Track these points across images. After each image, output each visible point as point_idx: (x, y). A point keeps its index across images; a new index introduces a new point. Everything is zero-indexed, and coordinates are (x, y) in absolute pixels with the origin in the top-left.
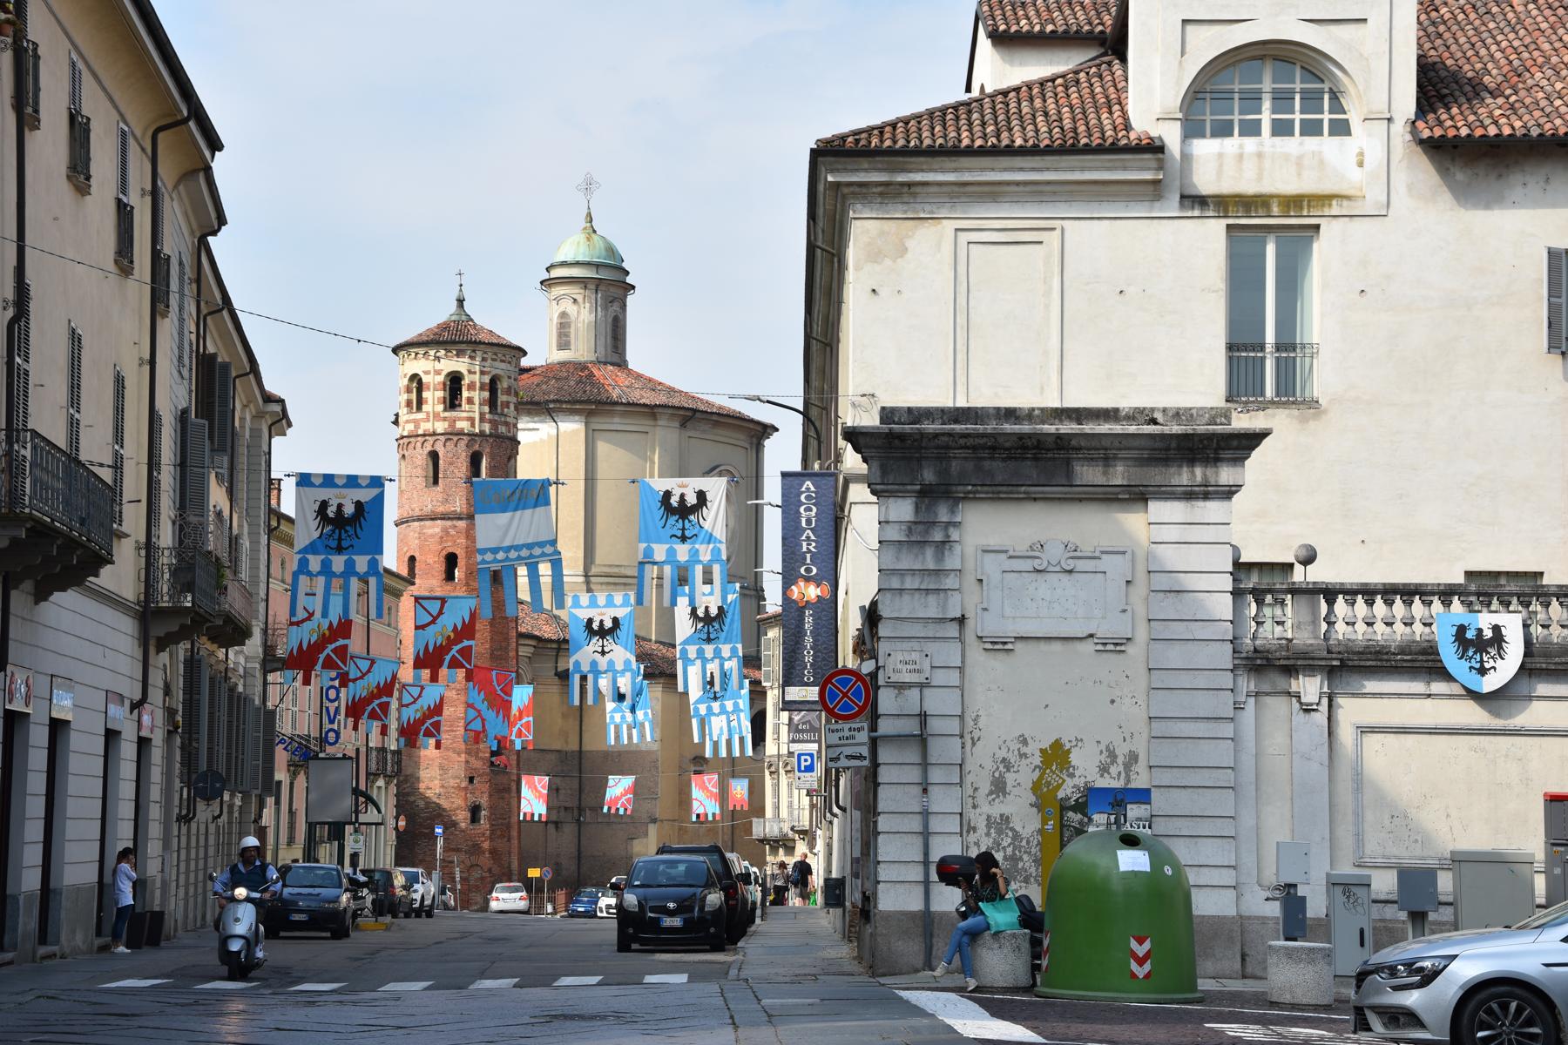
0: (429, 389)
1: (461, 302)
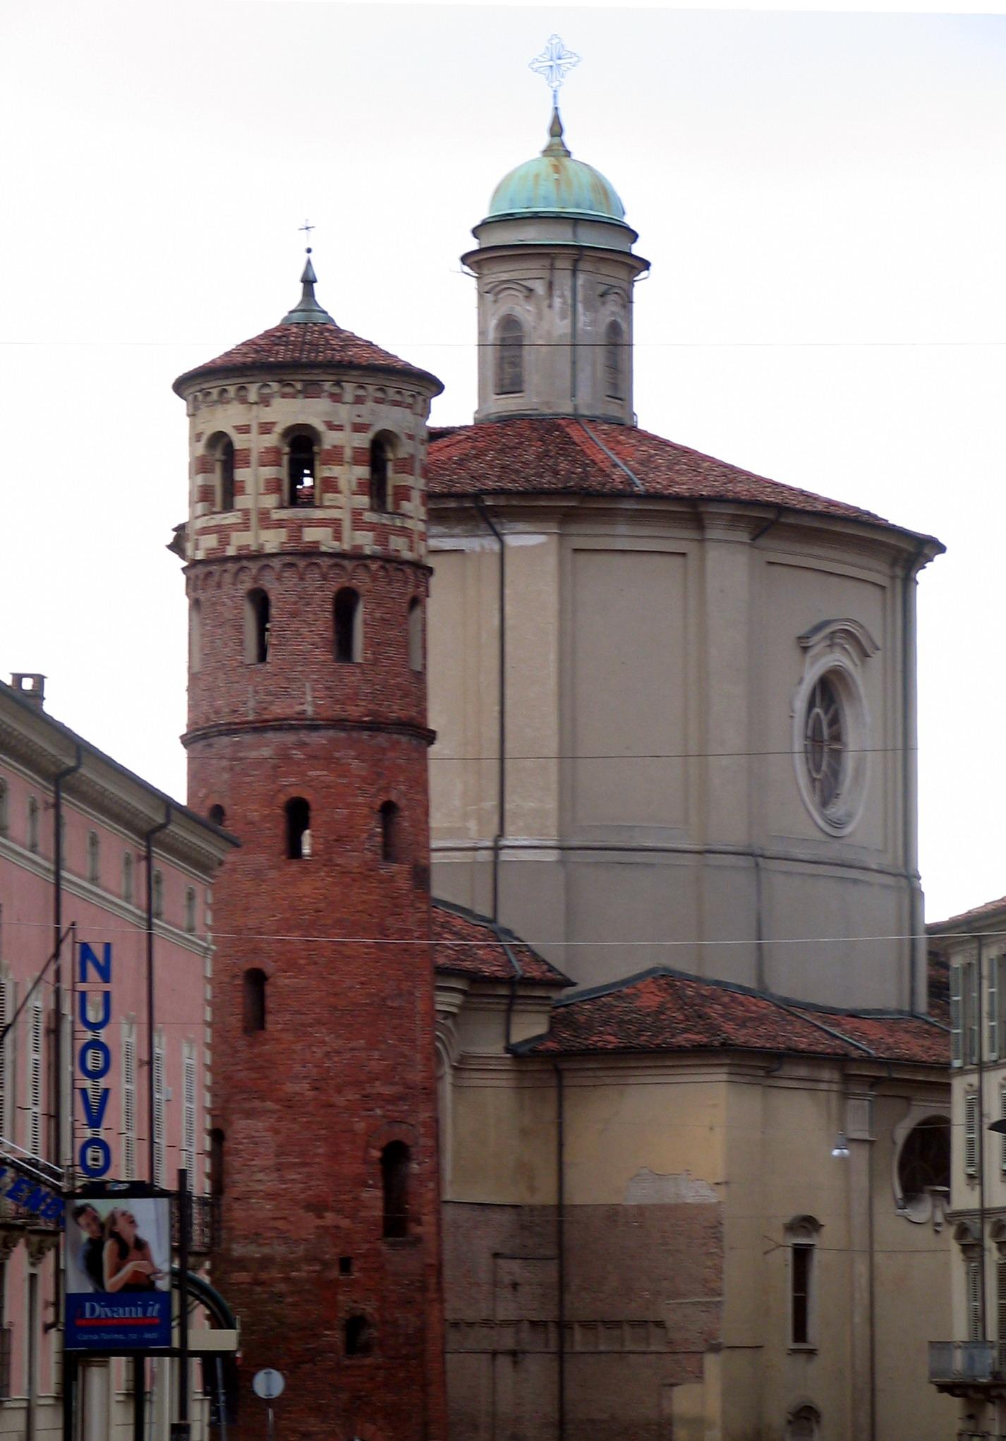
0: (247, 464)
1: (308, 282)
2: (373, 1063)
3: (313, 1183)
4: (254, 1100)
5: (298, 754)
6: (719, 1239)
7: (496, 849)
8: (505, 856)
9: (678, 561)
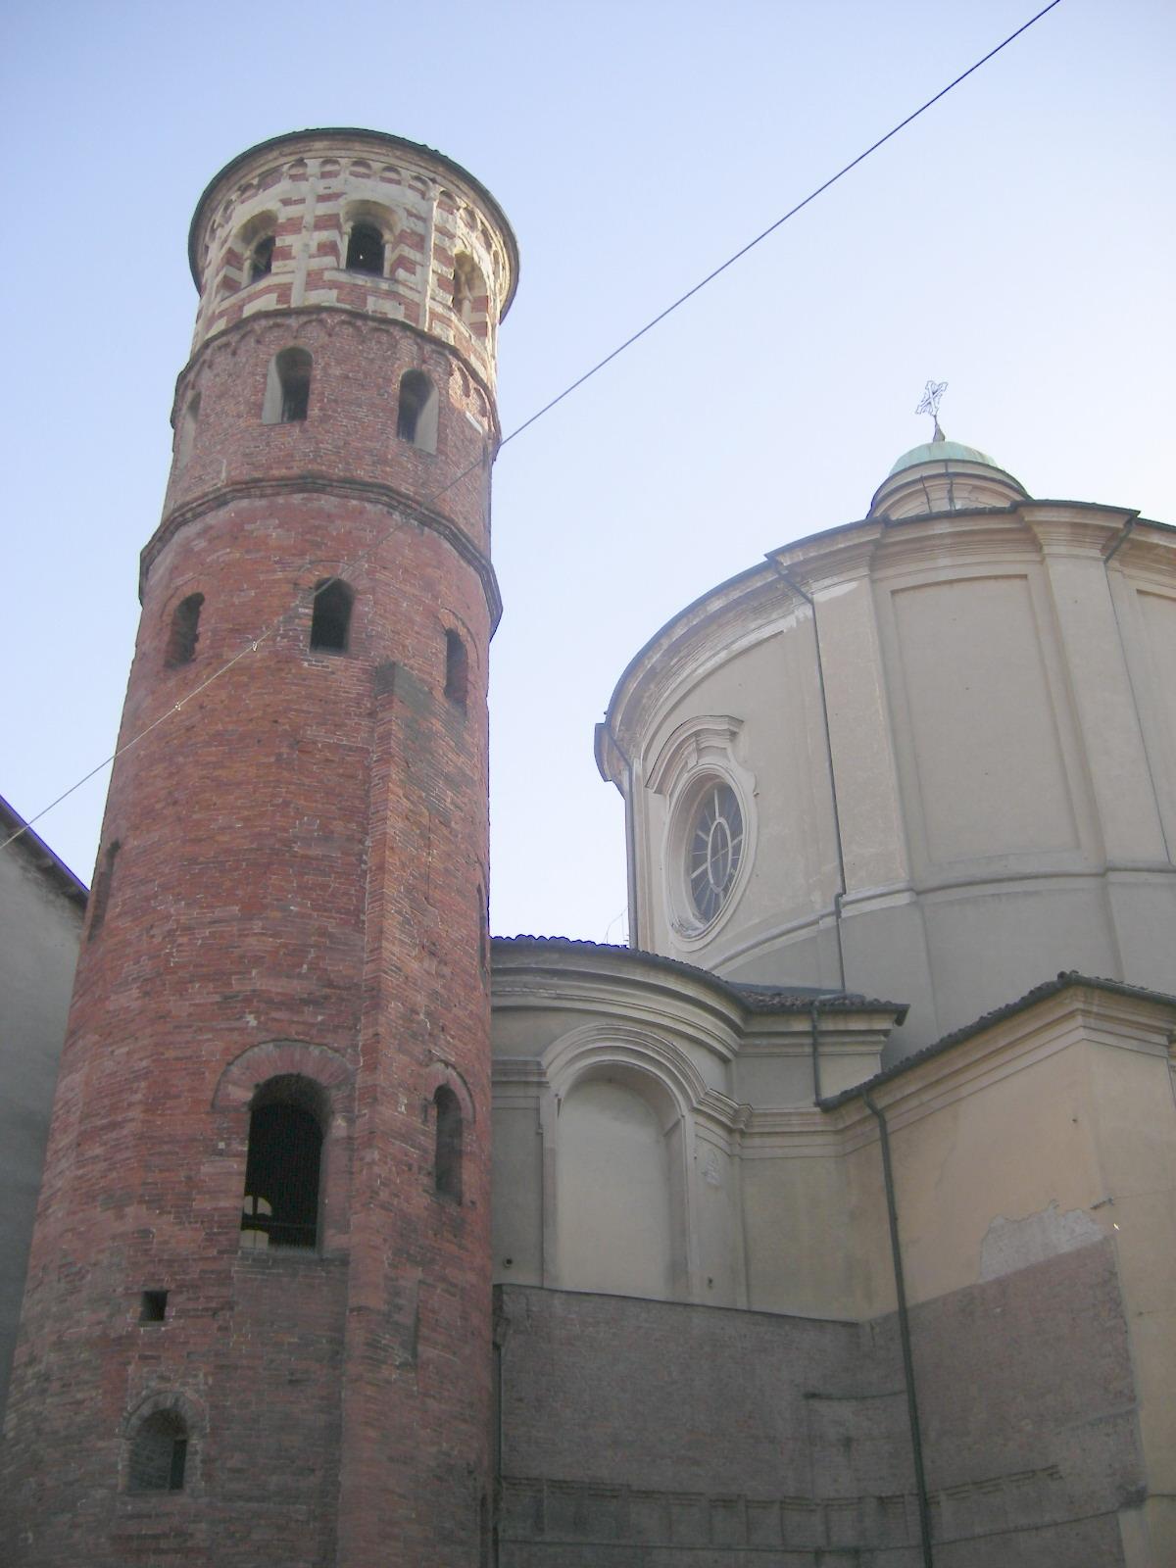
2: (252, 940)
3: (119, 1157)
4: (470, 1175)
5: (201, 544)
6: (1115, 1304)
7: (838, 913)
8: (845, 914)
9: (1018, 583)
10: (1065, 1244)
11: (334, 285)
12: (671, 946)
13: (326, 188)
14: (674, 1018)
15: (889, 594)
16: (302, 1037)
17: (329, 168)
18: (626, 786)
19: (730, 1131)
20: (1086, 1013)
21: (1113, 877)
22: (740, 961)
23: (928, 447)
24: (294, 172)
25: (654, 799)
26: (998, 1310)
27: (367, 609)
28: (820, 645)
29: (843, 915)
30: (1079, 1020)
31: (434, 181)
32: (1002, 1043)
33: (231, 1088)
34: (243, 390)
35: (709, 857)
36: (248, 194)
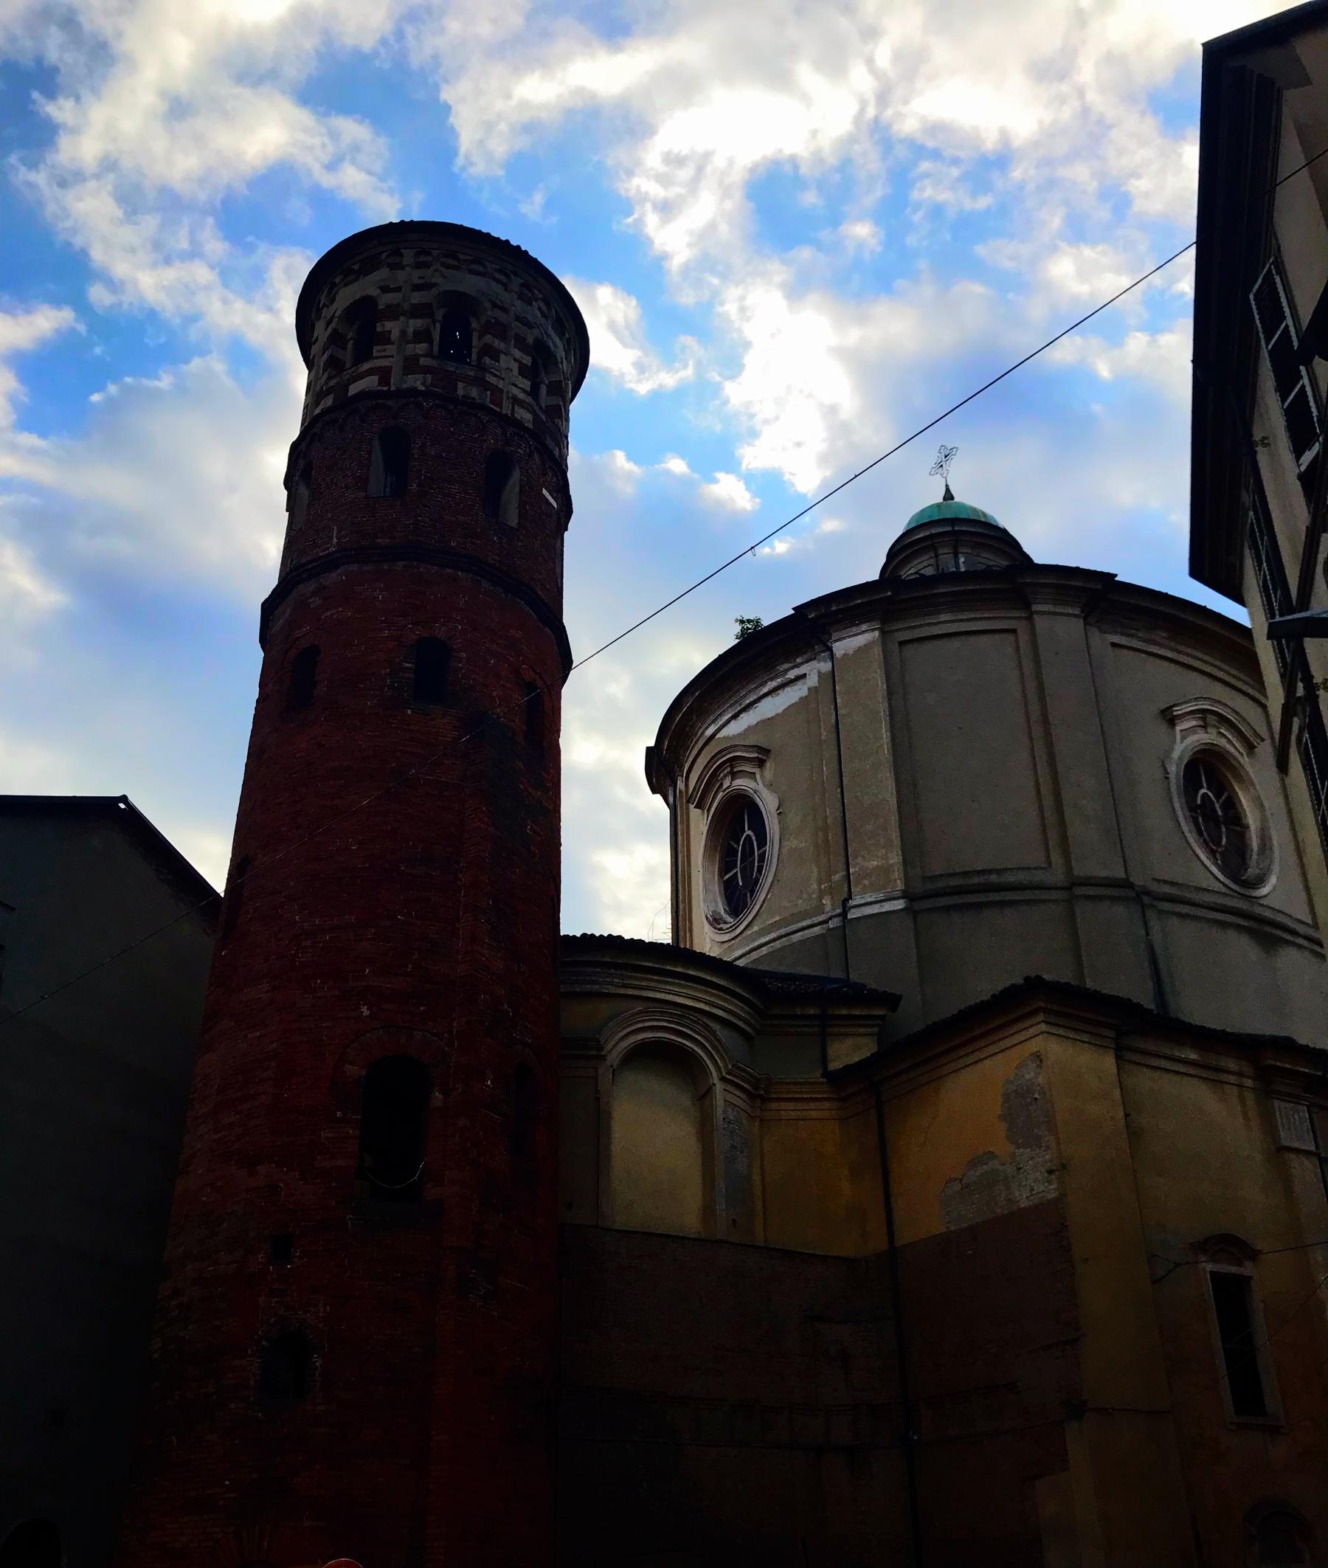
10: (1023, 1198)
11: (427, 370)
12: (707, 941)
13: (419, 278)
14: (706, 1003)
15: (897, 644)
16: (407, 1024)
17: (422, 258)
18: (671, 799)
19: (752, 1096)
20: (1045, 1010)
21: (1079, 891)
22: (764, 950)
23: (938, 505)
24: (390, 260)
25: (695, 813)
26: (970, 1252)
27: (460, 665)
28: (837, 688)
29: (849, 917)
30: (1041, 1017)
31: (516, 275)
32: (978, 1032)
33: (348, 1067)
34: (350, 464)
35: (739, 862)
36: (350, 278)
